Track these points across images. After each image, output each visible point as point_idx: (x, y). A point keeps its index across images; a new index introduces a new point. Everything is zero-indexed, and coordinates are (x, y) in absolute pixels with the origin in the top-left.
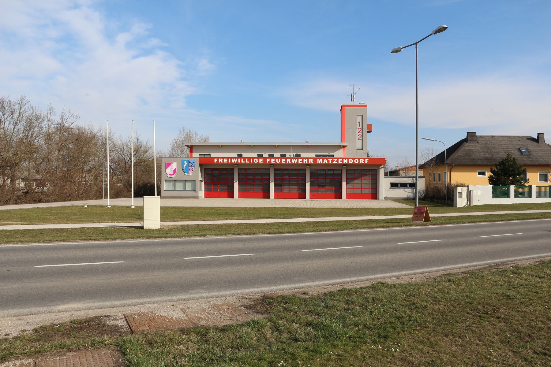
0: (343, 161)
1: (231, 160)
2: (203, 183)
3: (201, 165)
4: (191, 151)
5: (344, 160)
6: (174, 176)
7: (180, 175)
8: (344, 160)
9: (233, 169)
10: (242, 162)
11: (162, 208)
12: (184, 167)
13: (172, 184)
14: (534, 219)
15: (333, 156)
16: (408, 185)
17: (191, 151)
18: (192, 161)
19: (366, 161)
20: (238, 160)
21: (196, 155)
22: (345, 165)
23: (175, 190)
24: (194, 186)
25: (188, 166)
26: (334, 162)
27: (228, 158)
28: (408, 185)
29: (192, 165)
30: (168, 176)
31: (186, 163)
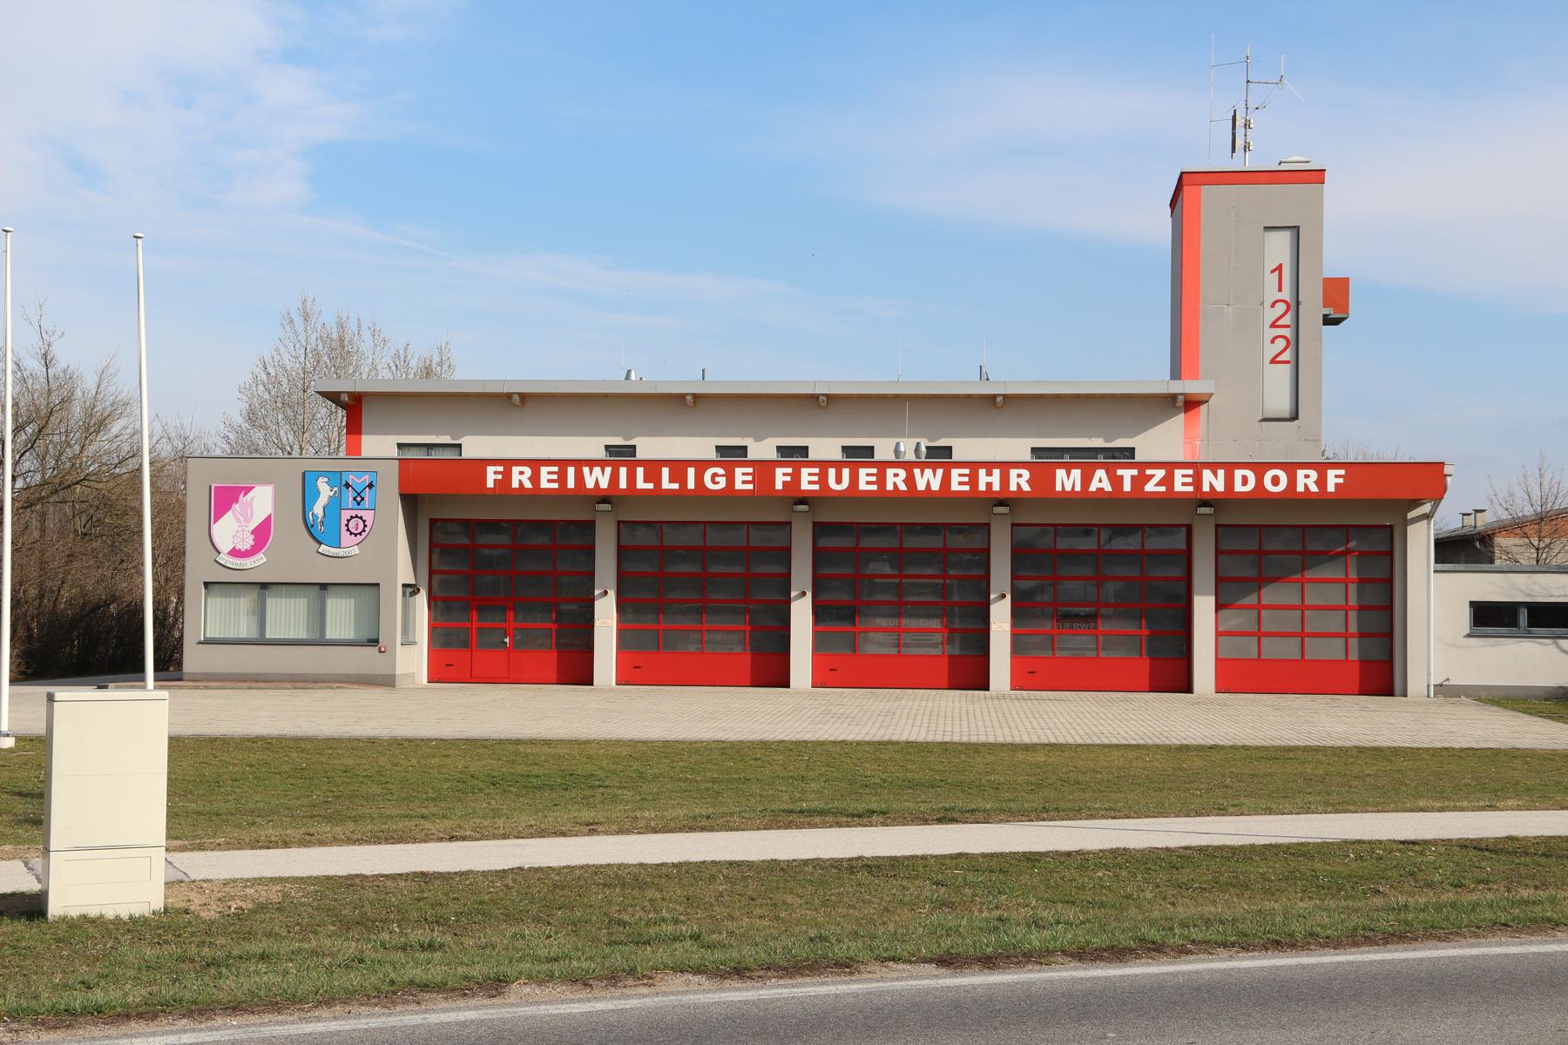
1: (579, 478)
2: (422, 600)
3: (411, 502)
4: (354, 427)
5: (1207, 475)
6: (260, 559)
7: (294, 557)
8: (1207, 475)
10: (641, 484)
11: (178, 746)
12: (318, 509)
13: (243, 604)
17: (354, 427)
18: (359, 482)
19: (1333, 479)
20: (614, 478)
21: (380, 445)
23: (262, 642)
24: (372, 614)
25: (335, 504)
26: (1150, 487)
29: (359, 499)
31: (325, 491)
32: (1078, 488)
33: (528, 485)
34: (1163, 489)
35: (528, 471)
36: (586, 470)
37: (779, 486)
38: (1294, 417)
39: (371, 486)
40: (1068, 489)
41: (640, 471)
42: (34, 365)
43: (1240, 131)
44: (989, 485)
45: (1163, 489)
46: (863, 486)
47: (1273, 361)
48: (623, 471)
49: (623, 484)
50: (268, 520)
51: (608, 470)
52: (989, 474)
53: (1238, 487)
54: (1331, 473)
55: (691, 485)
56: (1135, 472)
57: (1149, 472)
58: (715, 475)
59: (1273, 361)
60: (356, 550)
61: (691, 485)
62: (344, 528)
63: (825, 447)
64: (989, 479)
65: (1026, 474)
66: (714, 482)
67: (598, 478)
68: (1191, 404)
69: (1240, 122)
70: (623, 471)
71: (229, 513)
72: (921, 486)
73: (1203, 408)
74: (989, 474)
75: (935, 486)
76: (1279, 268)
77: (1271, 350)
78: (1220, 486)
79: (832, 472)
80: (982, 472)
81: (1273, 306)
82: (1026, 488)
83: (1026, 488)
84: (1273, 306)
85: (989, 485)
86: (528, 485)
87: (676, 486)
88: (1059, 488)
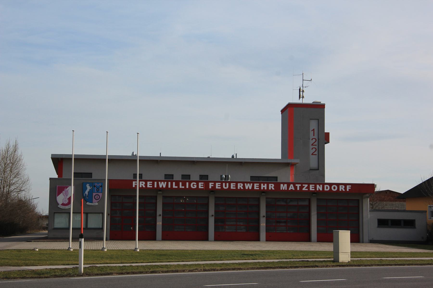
0: (315, 188)
1: (158, 185)
5: (318, 186)
8: (318, 186)
9: (258, 200)
10: (174, 187)
12: (87, 192)
14: (102, 275)
15: (276, 178)
16: (402, 223)
19: (348, 188)
20: (167, 185)
22: (264, 191)
25: (91, 192)
26: (304, 189)
27: (153, 181)
28: (402, 223)
29: (98, 189)
30: (60, 206)
31: (89, 188)
32: (286, 189)
33: (344, 190)
34: (307, 189)
35: (344, 187)
36: (160, 183)
37: (210, 187)
38: (318, 169)
39: (101, 186)
40: (284, 189)
41: (174, 183)
42: (11, 149)
43: (301, 93)
44: (264, 188)
45: (307, 189)
46: (232, 188)
47: (312, 154)
48: (169, 183)
49: (169, 187)
50: (58, 195)
51: (166, 183)
52: (264, 185)
53: (325, 189)
54: (348, 186)
55: (187, 187)
56: (300, 185)
57: (304, 185)
58: (194, 184)
59: (312, 154)
60: (97, 204)
61: (187, 187)
62: (94, 198)
63: (195, 177)
64: (264, 186)
65: (273, 185)
66: (193, 186)
67: (162, 185)
68: (292, 165)
69: (301, 91)
70: (169, 183)
71: (62, 194)
72: (247, 188)
73: (295, 166)
74: (264, 185)
75: (250, 188)
76: (314, 130)
77: (312, 151)
78: (321, 189)
79: (224, 184)
80: (262, 185)
81: (312, 140)
82: (273, 189)
83: (273, 189)
84: (312, 140)
85: (264, 188)
86: (344, 190)
87: (183, 187)
88: (281, 189)
